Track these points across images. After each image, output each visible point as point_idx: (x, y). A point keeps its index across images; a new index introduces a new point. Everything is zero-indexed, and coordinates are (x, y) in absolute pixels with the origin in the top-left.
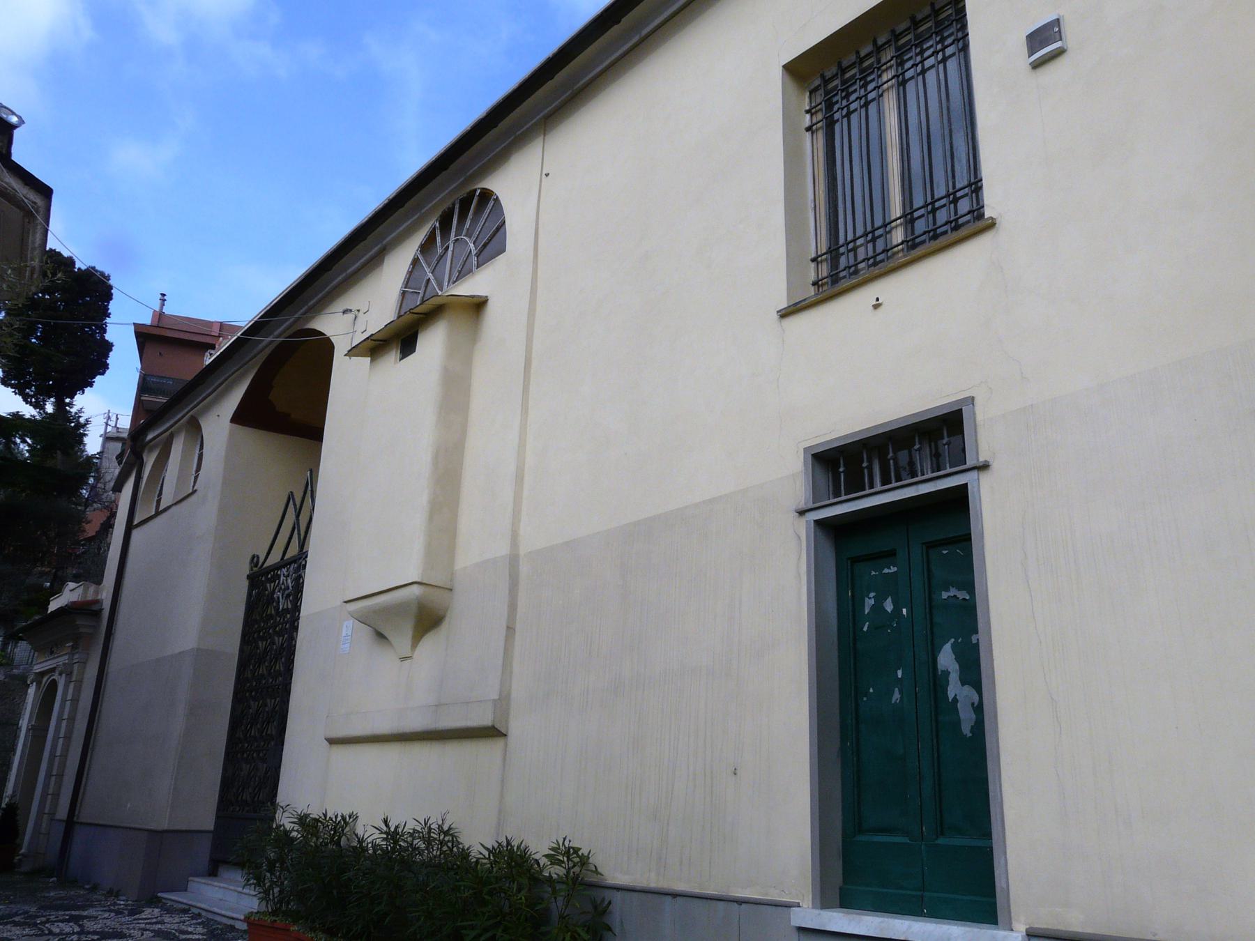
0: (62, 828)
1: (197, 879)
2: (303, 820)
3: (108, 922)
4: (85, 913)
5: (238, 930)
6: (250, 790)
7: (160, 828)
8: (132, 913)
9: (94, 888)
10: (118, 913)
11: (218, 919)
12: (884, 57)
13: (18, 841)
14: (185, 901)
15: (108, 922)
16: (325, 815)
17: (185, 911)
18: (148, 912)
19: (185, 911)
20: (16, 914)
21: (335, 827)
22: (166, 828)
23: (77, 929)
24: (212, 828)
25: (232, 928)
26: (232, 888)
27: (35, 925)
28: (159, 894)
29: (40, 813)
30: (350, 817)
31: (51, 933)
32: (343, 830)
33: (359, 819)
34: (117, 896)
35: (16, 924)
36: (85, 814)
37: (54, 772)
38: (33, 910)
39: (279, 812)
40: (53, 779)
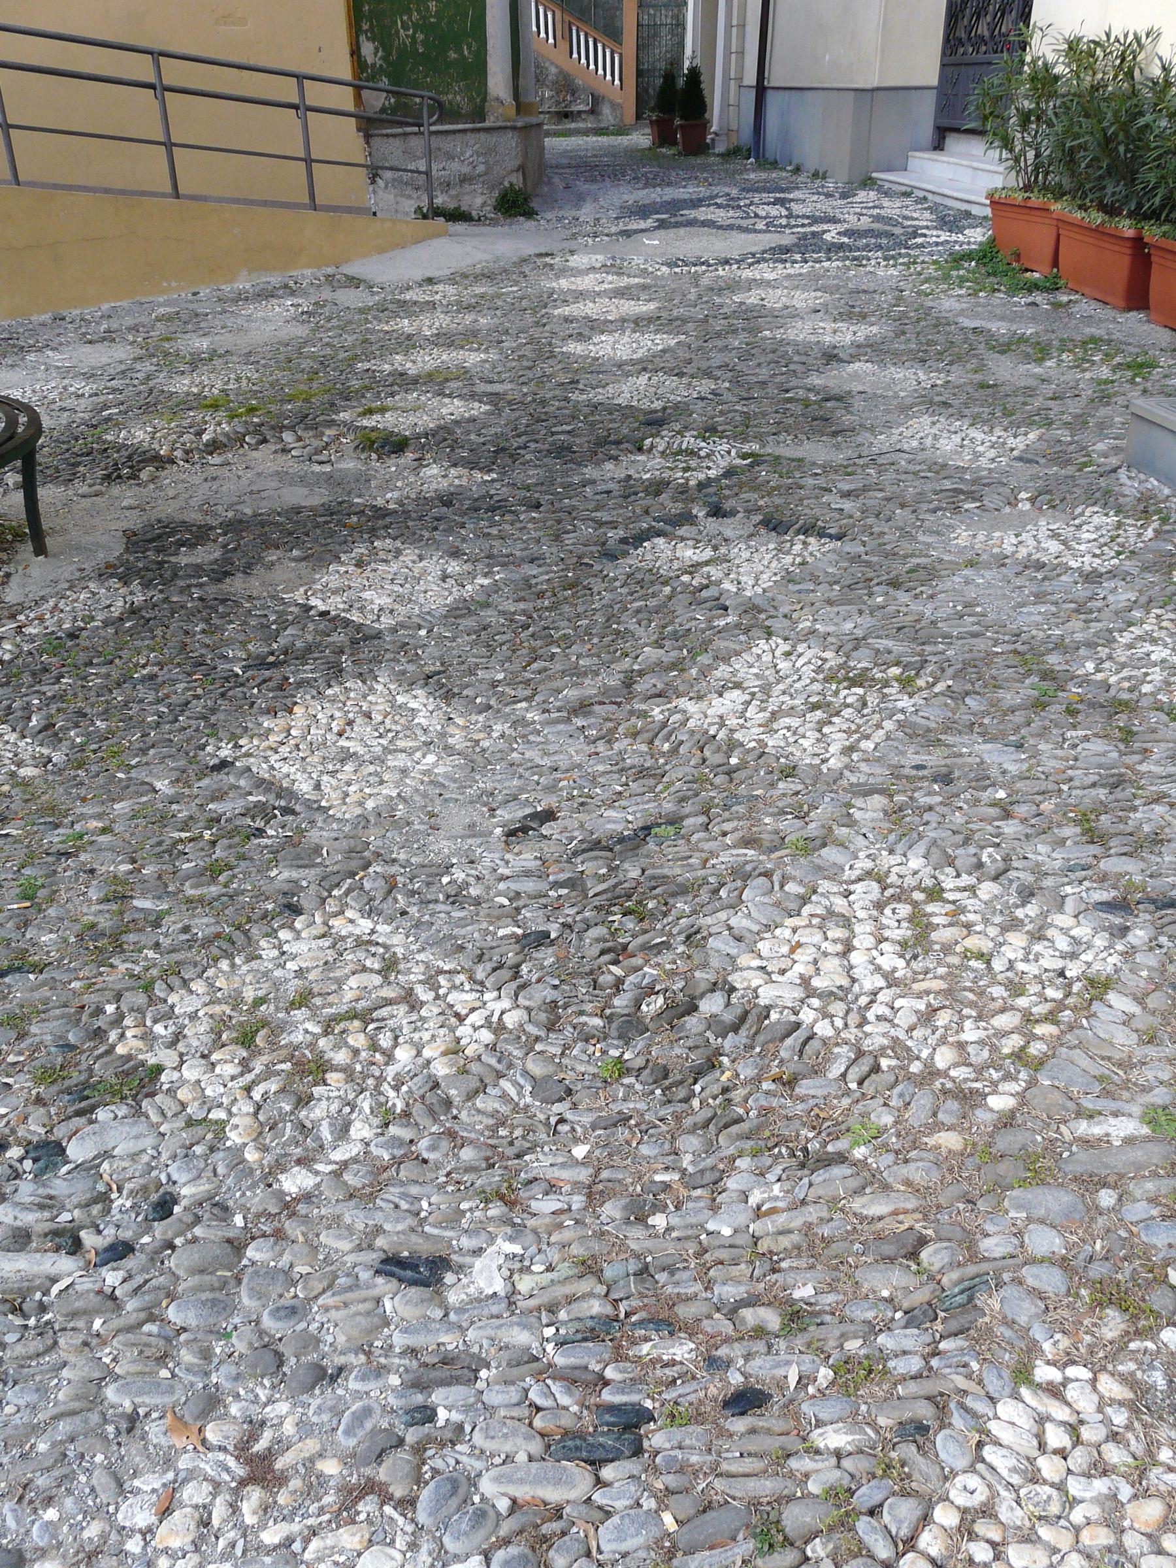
0: (752, 95)
1: (917, 154)
2: (1073, 47)
3: (819, 206)
4: (791, 196)
5: (975, 217)
6: (989, 18)
7: (869, 86)
8: (844, 196)
9: (797, 170)
10: (828, 195)
11: (949, 202)
12: (408, 1312)
13: (707, 116)
14: (906, 182)
15: (819, 206)
16: (1108, 35)
17: (906, 195)
18: (862, 195)
19: (906, 195)
20: (717, 196)
21: (1124, 52)
22: (875, 85)
23: (784, 212)
24: (935, 82)
25: (968, 214)
26: (965, 163)
27: (739, 207)
28: (874, 175)
29: (726, 78)
30: (1148, 36)
31: (757, 216)
32: (1134, 58)
33: (1162, 38)
34: (824, 178)
35: (719, 206)
36: (777, 76)
37: (735, 22)
38: (734, 192)
39: (1037, 35)
40: (734, 30)
